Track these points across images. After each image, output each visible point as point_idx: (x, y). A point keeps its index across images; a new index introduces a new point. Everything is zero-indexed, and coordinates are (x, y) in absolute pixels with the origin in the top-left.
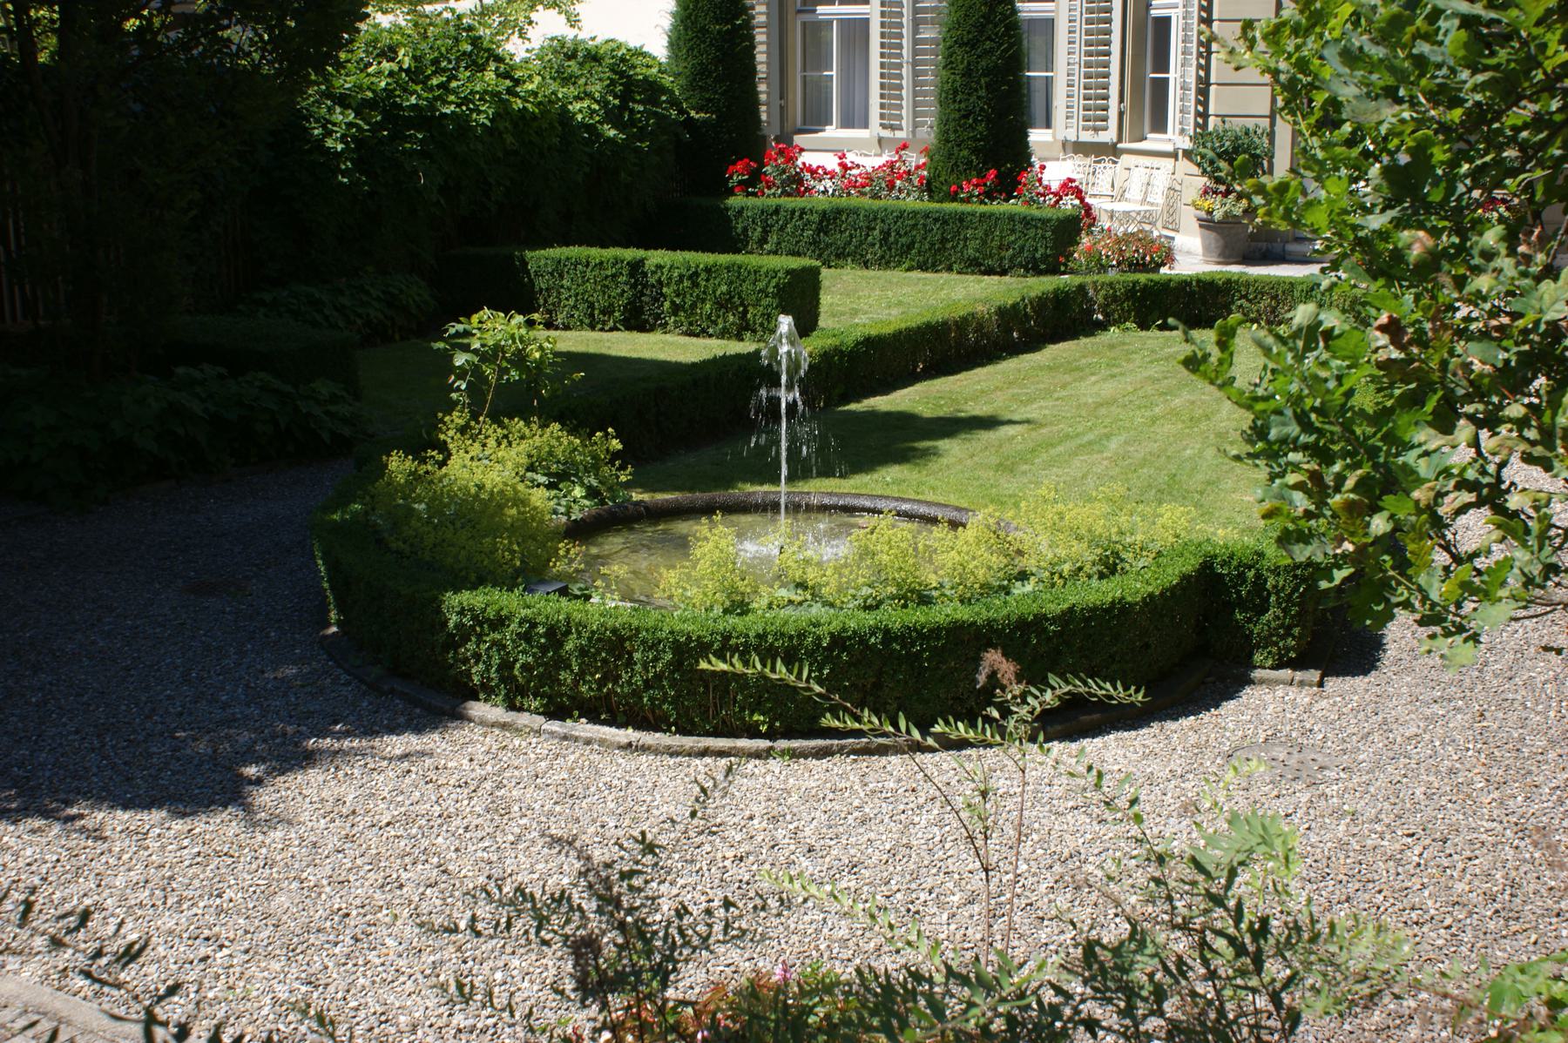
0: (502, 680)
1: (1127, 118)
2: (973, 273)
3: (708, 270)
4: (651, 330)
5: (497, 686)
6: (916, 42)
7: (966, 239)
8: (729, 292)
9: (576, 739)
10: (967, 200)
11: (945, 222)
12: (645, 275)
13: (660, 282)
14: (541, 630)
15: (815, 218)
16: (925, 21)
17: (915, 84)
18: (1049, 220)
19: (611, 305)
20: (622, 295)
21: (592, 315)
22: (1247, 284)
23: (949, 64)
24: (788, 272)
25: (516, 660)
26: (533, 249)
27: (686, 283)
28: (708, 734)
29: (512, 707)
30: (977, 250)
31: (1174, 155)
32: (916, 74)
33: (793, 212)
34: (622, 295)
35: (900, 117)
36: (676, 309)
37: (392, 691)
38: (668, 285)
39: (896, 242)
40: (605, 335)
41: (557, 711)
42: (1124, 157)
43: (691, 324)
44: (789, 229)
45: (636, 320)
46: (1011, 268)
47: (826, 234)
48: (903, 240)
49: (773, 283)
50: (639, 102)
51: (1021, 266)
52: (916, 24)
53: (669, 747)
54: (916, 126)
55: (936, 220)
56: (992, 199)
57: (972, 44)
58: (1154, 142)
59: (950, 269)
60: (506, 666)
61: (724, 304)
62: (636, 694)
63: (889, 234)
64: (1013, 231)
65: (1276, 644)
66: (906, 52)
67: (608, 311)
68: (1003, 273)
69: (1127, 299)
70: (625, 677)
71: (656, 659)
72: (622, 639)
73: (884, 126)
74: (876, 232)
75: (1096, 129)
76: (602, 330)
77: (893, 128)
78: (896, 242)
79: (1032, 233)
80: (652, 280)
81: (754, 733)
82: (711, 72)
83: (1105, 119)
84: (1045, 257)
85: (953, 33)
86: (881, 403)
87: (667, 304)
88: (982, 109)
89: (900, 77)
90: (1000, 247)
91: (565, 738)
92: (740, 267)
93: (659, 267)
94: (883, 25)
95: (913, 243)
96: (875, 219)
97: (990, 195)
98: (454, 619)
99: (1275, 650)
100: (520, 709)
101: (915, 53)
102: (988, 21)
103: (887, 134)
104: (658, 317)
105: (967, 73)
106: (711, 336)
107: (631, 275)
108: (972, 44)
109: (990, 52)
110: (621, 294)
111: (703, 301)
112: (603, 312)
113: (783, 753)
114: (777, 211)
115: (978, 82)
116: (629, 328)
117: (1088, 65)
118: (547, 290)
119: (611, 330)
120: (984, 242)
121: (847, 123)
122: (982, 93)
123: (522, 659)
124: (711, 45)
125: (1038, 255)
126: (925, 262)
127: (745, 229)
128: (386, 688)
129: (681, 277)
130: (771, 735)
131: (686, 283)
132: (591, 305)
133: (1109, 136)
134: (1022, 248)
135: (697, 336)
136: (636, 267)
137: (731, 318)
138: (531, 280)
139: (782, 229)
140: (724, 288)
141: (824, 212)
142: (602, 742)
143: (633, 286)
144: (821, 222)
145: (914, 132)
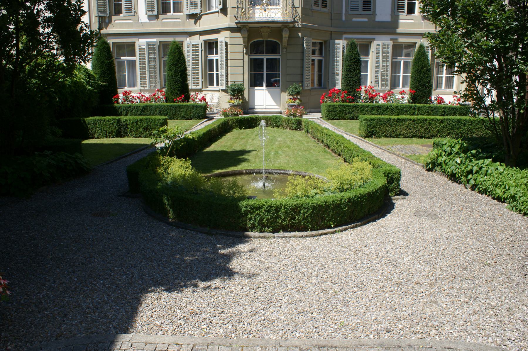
0: (259, 224)
3: (141, 120)
4: (124, 137)
9: (286, 237)
10: (178, 102)
11: (176, 108)
12: (121, 122)
13: (127, 124)
14: (273, 208)
16: (151, 61)
17: (150, 76)
29: (261, 232)
32: (150, 73)
35: (146, 84)
36: (131, 132)
37: (216, 233)
38: (129, 125)
41: (275, 231)
44: (133, 111)
45: (119, 135)
54: (150, 86)
56: (183, 102)
58: (215, 87)
59: (177, 119)
60: (262, 220)
61: (146, 129)
62: (300, 222)
66: (147, 68)
67: (111, 133)
68: (191, 119)
70: (297, 217)
71: (307, 212)
72: (297, 208)
73: (142, 86)
75: (196, 86)
77: (144, 87)
79: (198, 109)
80: (124, 124)
81: (330, 227)
84: (202, 115)
87: (129, 130)
90: (190, 113)
91: (283, 237)
93: (126, 120)
94: (140, 62)
97: (183, 101)
98: (244, 209)
100: (264, 232)
101: (149, 68)
103: (142, 88)
105: (175, 72)
107: (118, 123)
109: (180, 66)
111: (139, 128)
112: (109, 133)
116: (117, 137)
117: (193, 71)
120: (186, 112)
122: (179, 76)
127: (121, 112)
129: (133, 122)
130: (335, 227)
132: (106, 132)
133: (200, 87)
136: (119, 120)
138: (87, 126)
139: (132, 111)
140: (146, 125)
142: (294, 237)
143: (119, 126)
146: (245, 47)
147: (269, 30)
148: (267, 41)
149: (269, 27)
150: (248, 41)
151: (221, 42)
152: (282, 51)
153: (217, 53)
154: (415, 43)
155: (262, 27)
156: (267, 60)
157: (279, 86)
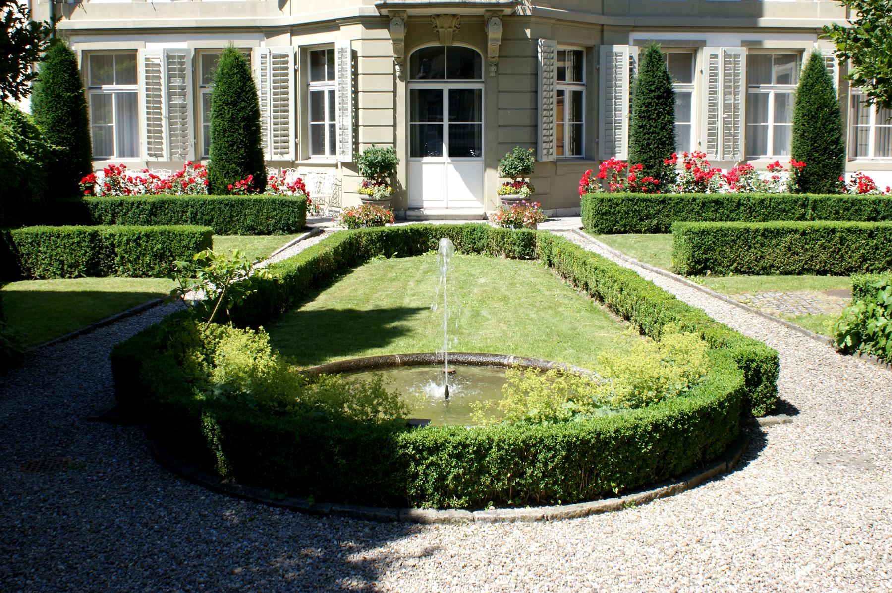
1: (300, 147)
2: (250, 234)
4: (106, 275)
5: (432, 494)
6: (170, 106)
7: (246, 215)
8: (162, 248)
9: (504, 520)
11: (232, 206)
12: (100, 241)
13: (113, 245)
15: (148, 207)
18: (296, 202)
19: (77, 261)
20: (84, 254)
21: (62, 269)
22: (436, 230)
23: (219, 115)
24: (202, 234)
25: (449, 473)
26: (14, 229)
27: (132, 244)
28: (580, 501)
30: (253, 221)
31: (336, 166)
32: (171, 124)
33: (133, 204)
34: (84, 254)
35: (161, 149)
38: (119, 246)
39: (202, 219)
40: (73, 280)
41: (475, 505)
42: (300, 168)
43: (135, 270)
44: (130, 214)
45: (94, 270)
46: (274, 230)
47: (155, 216)
48: (206, 217)
49: (193, 240)
50: (31, 138)
51: (280, 229)
52: (170, 96)
53: (568, 513)
54: (172, 154)
55: (227, 205)
56: (251, 192)
57: (234, 104)
58: (327, 157)
59: (236, 233)
60: (442, 477)
61: (160, 256)
62: (536, 483)
63: (196, 214)
64: (275, 209)
65: (764, 402)
68: (269, 233)
69: (378, 241)
70: (529, 471)
71: (553, 457)
73: (150, 155)
74: (189, 214)
76: (70, 278)
77: (156, 156)
78: (202, 219)
79: (286, 209)
80: (107, 244)
81: (609, 495)
82: (65, 122)
83: (288, 147)
84: (295, 223)
85: (222, 98)
86: (309, 307)
87: (118, 259)
88: (242, 141)
89: (161, 126)
90: (267, 219)
91: (495, 521)
92: (169, 232)
95: (212, 219)
96: (187, 206)
97: (250, 190)
99: (763, 406)
100: (449, 507)
101: (170, 112)
102: (243, 91)
103: (153, 159)
104: (110, 267)
106: (150, 277)
107: (91, 241)
108: (234, 104)
110: (83, 255)
111: (144, 255)
112: (70, 266)
113: (630, 504)
114: (121, 204)
115: (239, 125)
118: (27, 254)
119: (76, 277)
120: (257, 216)
121: (122, 154)
122: (241, 131)
123: (455, 471)
124: (64, 105)
125: (290, 222)
126: (221, 230)
127: (100, 216)
128: (326, 511)
129: (128, 241)
131: (132, 244)
132: (62, 262)
133: (290, 157)
134: (281, 218)
135: (141, 277)
136: (94, 236)
137: (164, 265)
139: (125, 214)
140: (159, 246)
141: (154, 203)
143: (93, 248)
144: (152, 209)
145: (171, 158)
146: (399, 62)
147: (455, 22)
148: (451, 49)
149: (454, 16)
150: (407, 48)
151: (342, 50)
152: (487, 72)
153: (332, 77)
154: (801, 51)
155: (438, 16)
156: (451, 92)
157: (479, 155)
